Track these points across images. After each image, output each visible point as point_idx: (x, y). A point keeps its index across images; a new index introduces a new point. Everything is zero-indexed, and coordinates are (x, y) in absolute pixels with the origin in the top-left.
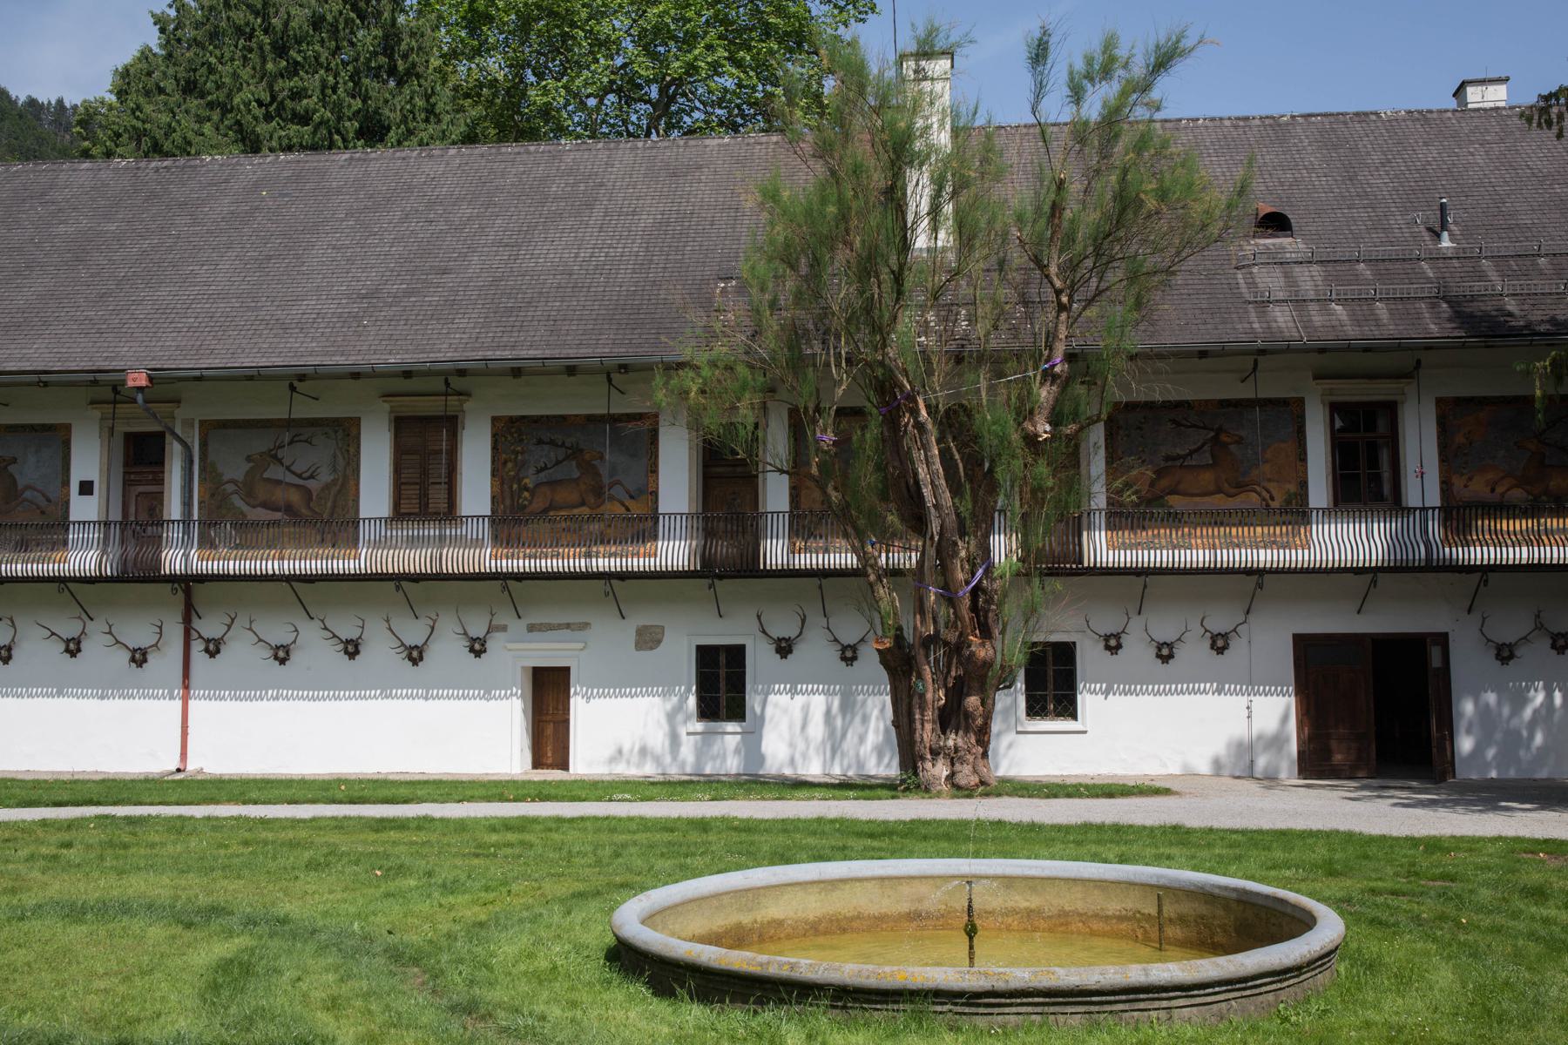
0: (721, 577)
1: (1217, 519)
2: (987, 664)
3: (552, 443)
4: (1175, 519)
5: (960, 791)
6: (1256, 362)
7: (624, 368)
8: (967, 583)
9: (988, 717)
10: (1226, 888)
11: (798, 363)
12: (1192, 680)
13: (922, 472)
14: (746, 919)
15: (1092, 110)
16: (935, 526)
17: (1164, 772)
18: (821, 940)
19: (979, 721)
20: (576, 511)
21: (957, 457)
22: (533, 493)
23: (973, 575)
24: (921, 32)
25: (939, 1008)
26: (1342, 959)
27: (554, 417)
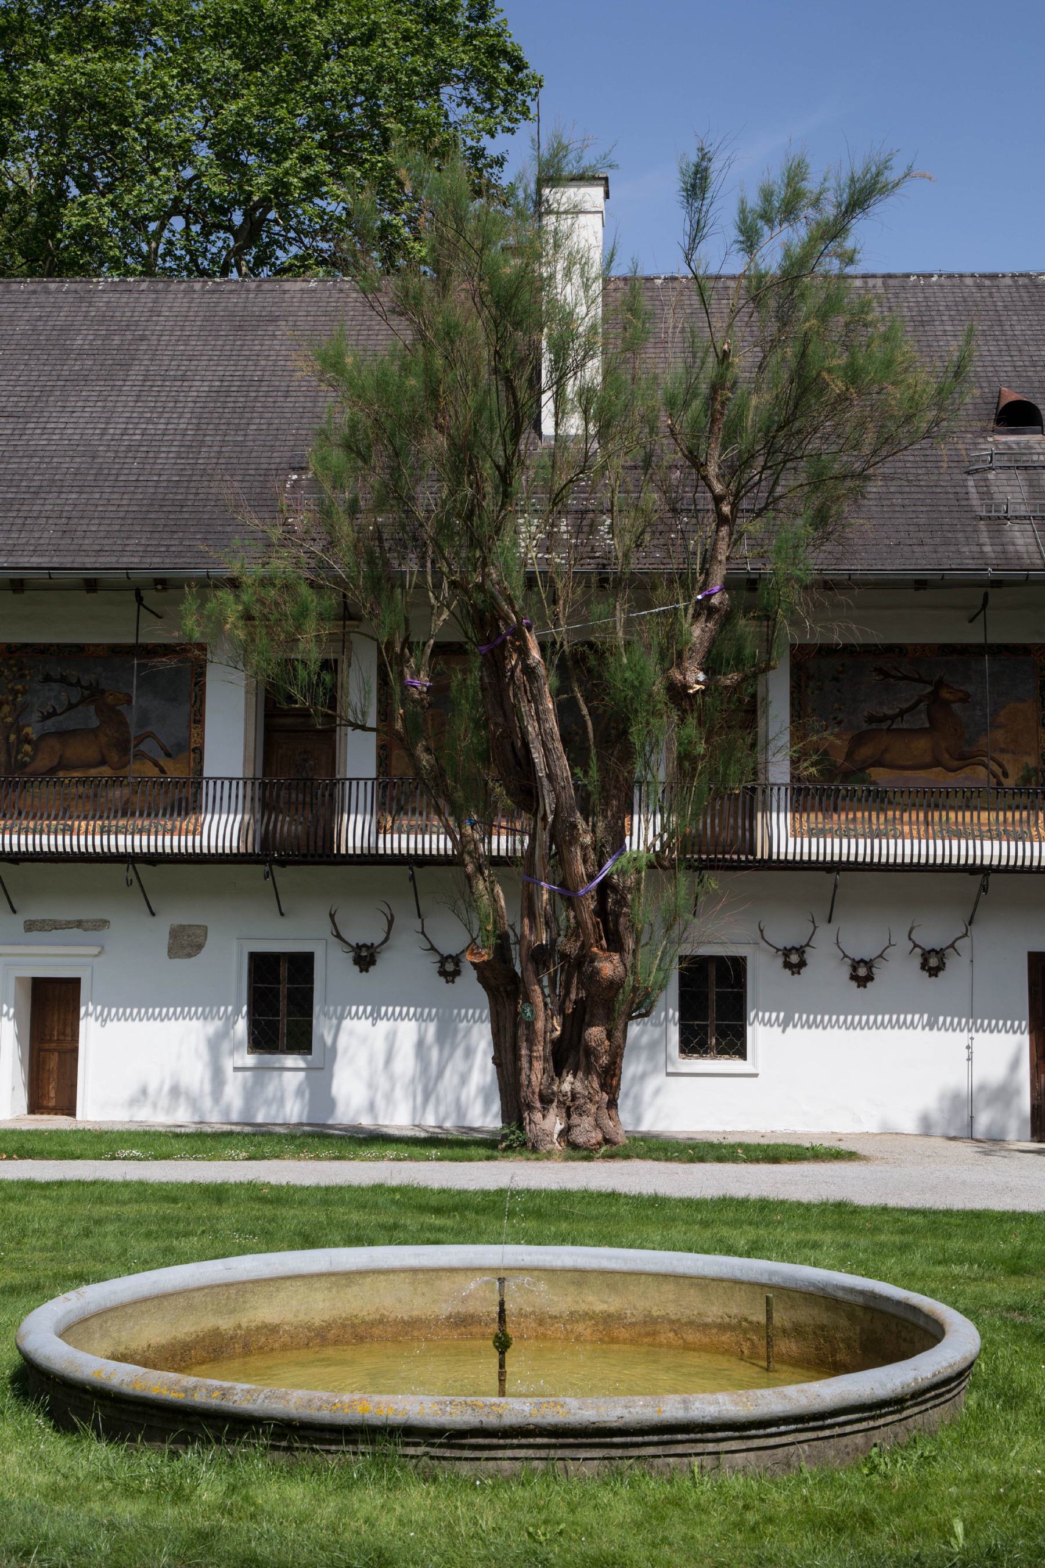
0: (283, 863)
1: (932, 800)
2: (615, 985)
3: (63, 680)
4: (879, 799)
5: (577, 1151)
6: (986, 595)
7: (162, 584)
8: (591, 877)
9: (616, 1055)
10: (852, 1290)
11: (382, 581)
12: (897, 1008)
13: (532, 728)
14: (225, 1324)
15: (771, 258)
16: (548, 802)
17: (857, 1129)
18: (330, 1352)
19: (604, 1060)
20: (93, 772)
21: (585, 711)
22: (36, 745)
23: (601, 866)
24: (545, 152)
25: (411, 1451)
26: (974, 1386)
27: (67, 646)
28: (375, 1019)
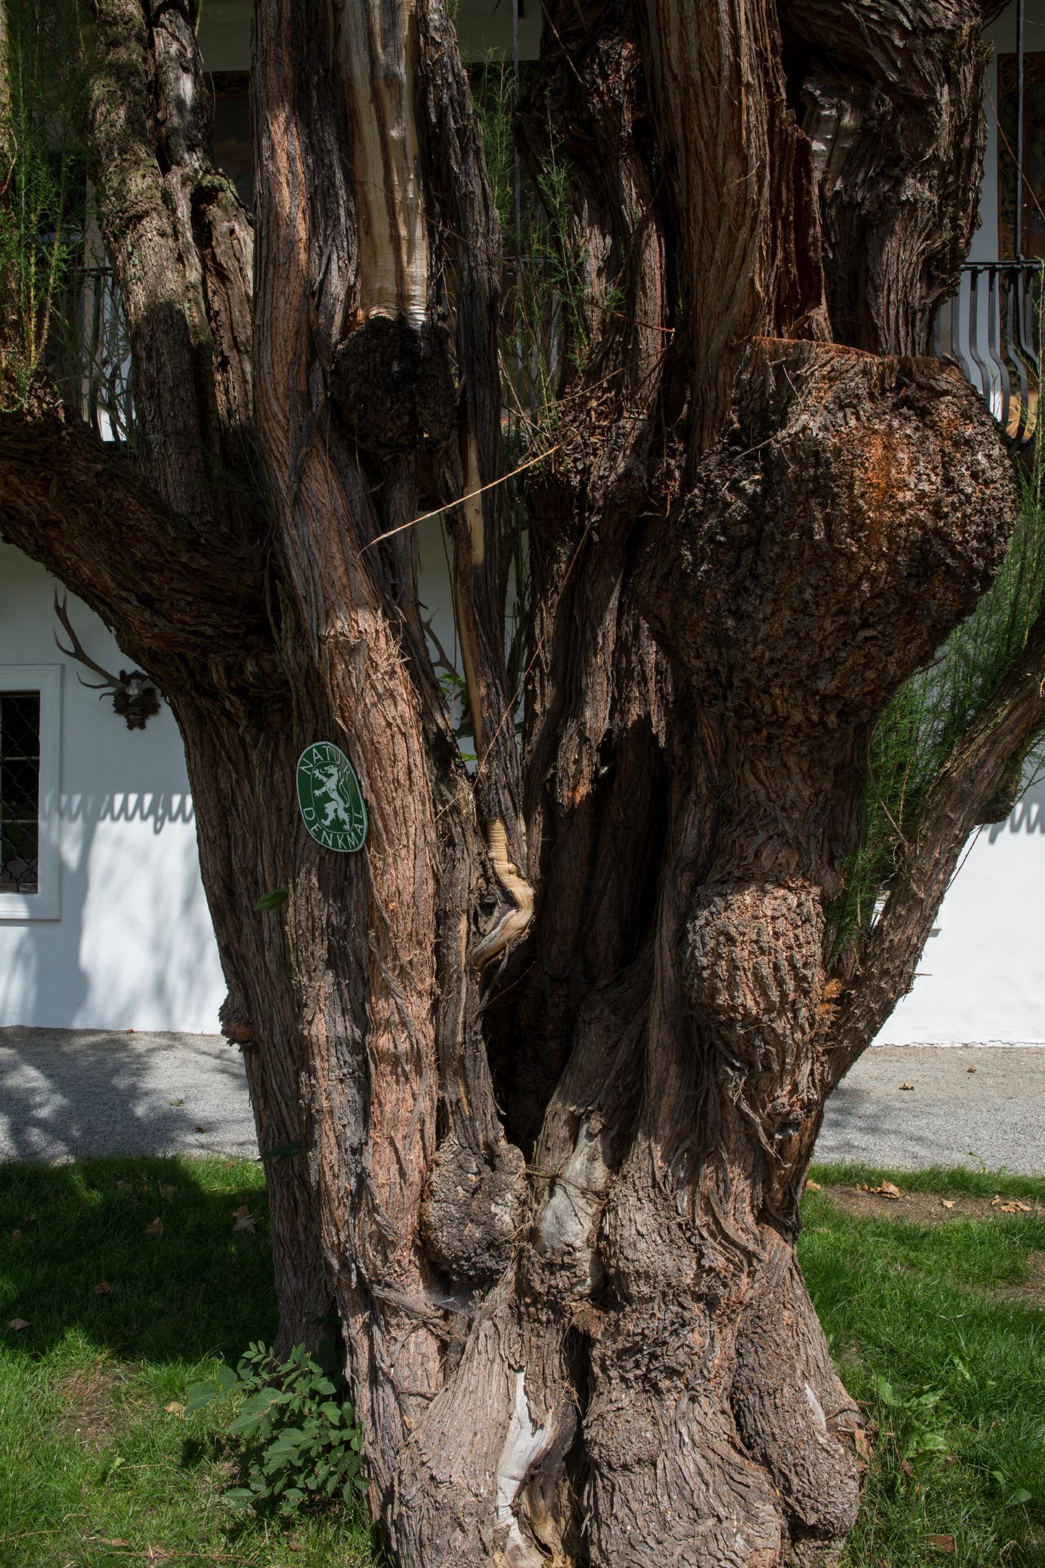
28: (159, 821)
